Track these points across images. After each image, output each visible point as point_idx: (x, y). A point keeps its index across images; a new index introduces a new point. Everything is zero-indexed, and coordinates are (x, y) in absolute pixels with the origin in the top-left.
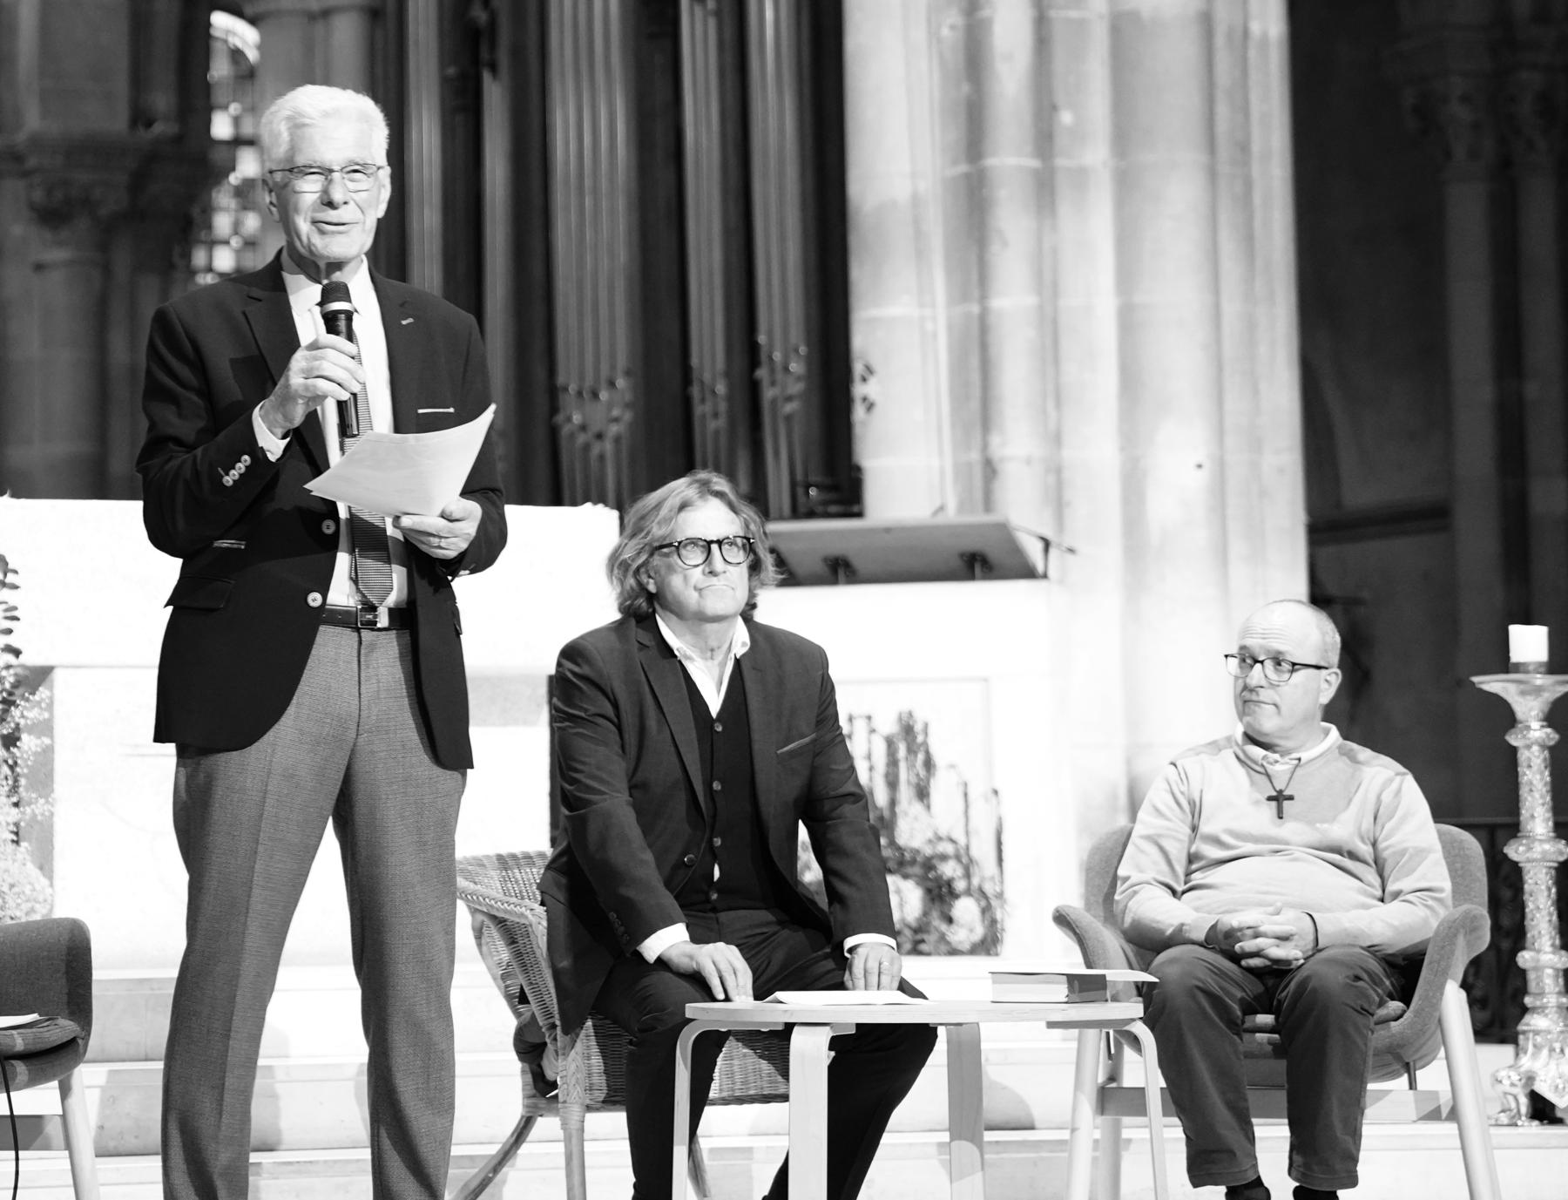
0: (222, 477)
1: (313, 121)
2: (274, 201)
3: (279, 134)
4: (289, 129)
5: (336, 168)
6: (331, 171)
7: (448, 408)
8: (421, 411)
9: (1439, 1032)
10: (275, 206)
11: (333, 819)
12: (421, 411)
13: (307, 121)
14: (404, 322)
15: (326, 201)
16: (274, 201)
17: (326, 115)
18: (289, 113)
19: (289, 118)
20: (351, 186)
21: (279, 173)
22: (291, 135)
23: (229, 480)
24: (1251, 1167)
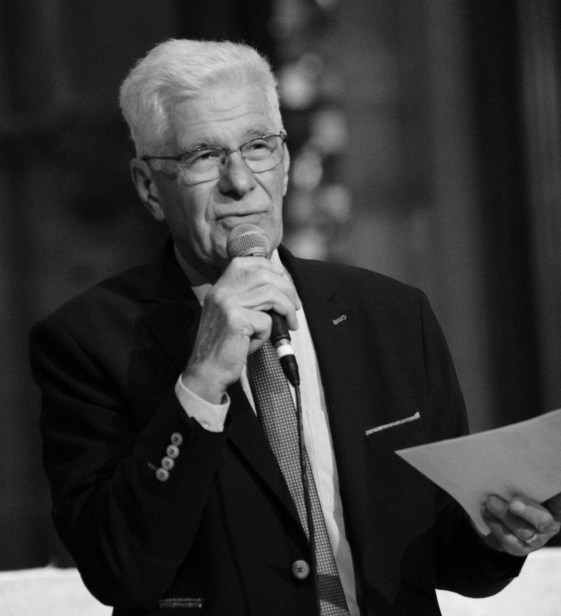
0: (154, 472)
1: (196, 93)
2: (154, 193)
3: (152, 109)
4: (164, 103)
5: (234, 145)
6: (227, 151)
7: (413, 415)
8: (369, 432)
9: (270, 254)
10: (155, 200)
11: (307, 539)
12: (369, 432)
13: (188, 92)
14: (336, 322)
15: (226, 187)
16: (154, 193)
17: (210, 82)
18: (160, 83)
19: (162, 90)
20: (253, 165)
21: (158, 160)
22: (167, 109)
23: (163, 473)
24: (149, 165)
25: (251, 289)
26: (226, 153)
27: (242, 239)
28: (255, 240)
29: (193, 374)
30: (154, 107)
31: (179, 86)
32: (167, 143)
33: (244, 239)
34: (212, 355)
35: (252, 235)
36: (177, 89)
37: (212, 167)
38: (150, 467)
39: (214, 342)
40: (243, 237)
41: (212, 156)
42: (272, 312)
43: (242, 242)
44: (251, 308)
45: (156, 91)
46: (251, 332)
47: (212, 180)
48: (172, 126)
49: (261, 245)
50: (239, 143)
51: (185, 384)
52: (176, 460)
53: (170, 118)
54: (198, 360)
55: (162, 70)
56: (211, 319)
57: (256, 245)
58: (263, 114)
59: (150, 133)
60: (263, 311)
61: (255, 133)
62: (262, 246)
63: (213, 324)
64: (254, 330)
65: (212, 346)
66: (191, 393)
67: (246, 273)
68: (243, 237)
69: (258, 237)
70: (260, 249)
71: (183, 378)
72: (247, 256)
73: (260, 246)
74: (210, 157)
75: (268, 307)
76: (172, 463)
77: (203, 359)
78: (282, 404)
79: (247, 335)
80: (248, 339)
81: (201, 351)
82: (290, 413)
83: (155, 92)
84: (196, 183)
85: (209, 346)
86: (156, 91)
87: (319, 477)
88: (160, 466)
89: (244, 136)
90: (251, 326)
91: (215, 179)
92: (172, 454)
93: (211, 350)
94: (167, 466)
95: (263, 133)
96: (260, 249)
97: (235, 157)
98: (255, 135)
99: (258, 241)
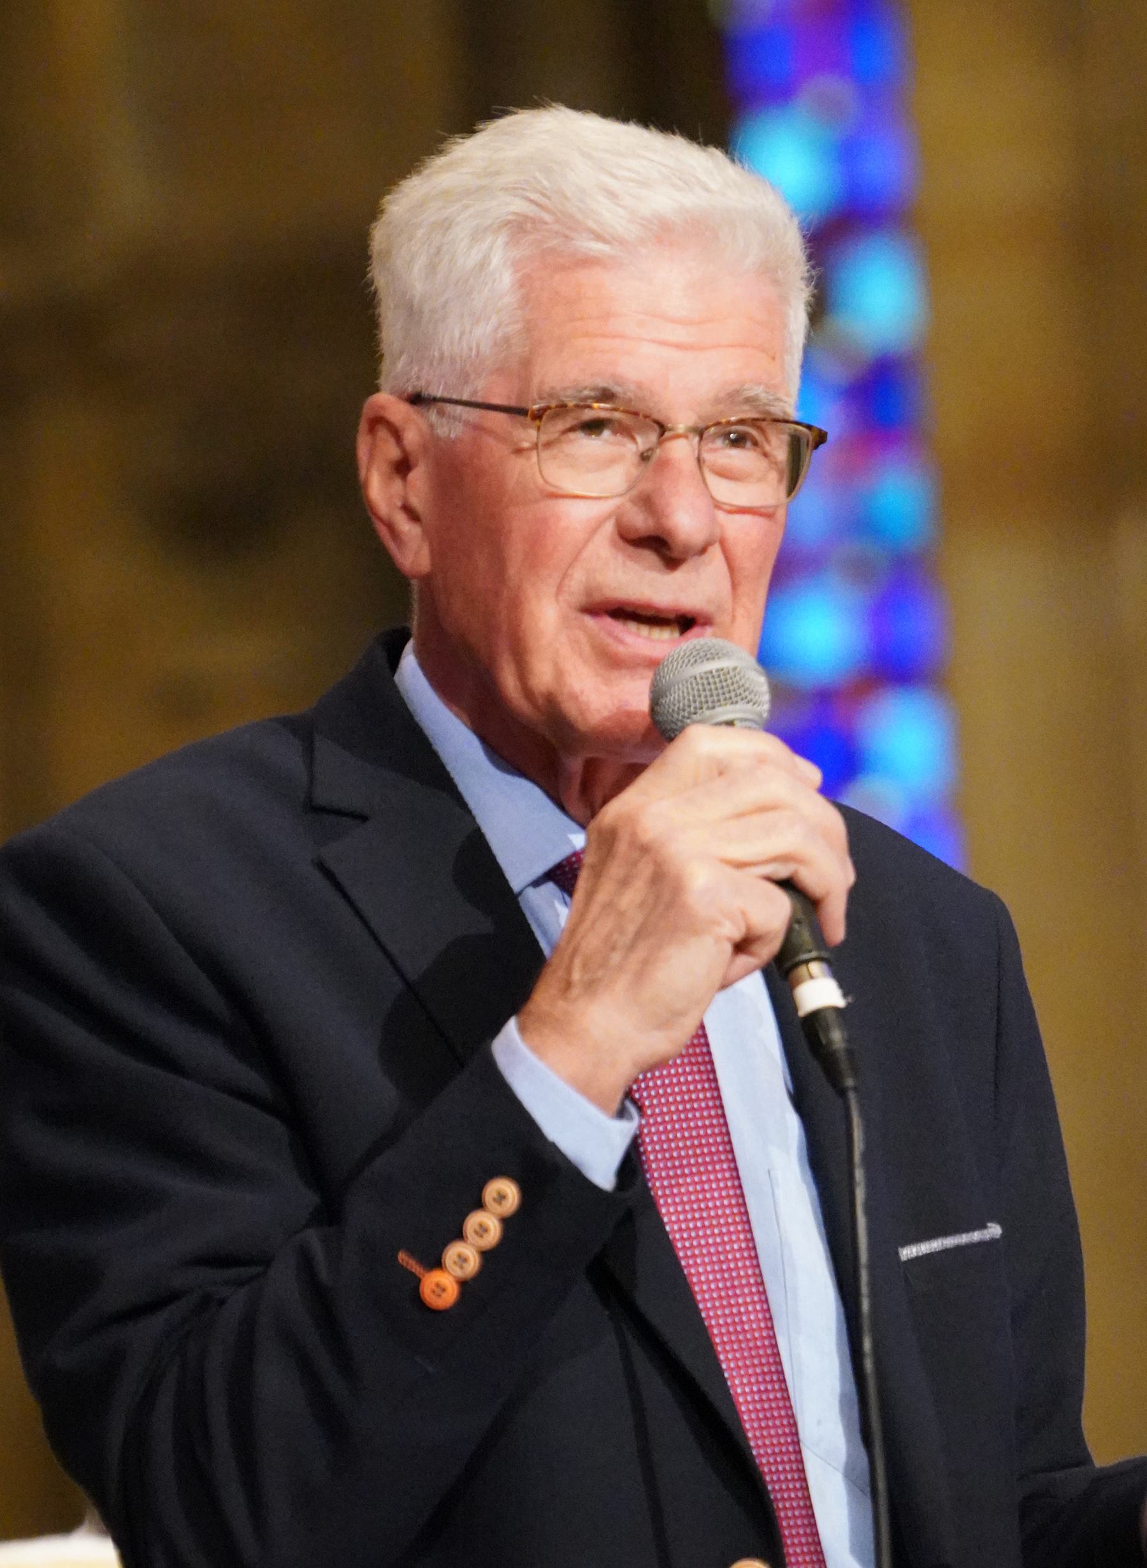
4: (516, 265)
5: (682, 421)
15: (640, 522)
18: (519, 206)
19: (519, 227)
22: (524, 283)
25: (740, 815)
26: (662, 434)
27: (707, 678)
28: (743, 686)
29: (561, 1026)
30: (489, 264)
31: (570, 225)
32: (500, 371)
33: (713, 677)
34: (622, 983)
35: (735, 669)
36: (567, 232)
37: (612, 461)
38: (405, 1264)
39: (632, 947)
40: (711, 672)
41: (615, 432)
42: (788, 885)
43: (707, 687)
44: (740, 865)
45: (506, 225)
46: (737, 934)
47: (607, 498)
48: (529, 328)
49: (749, 698)
50: (700, 417)
51: (535, 1049)
52: (486, 1255)
53: (526, 301)
54: (575, 992)
55: (538, 174)
56: (625, 883)
57: (742, 699)
58: (774, 358)
59: (457, 334)
60: (769, 879)
61: (748, 400)
62: (751, 700)
63: (630, 898)
64: (748, 928)
65: (626, 957)
66: (553, 1078)
67: (721, 769)
68: (711, 672)
69: (739, 674)
70: (744, 712)
71: (522, 1029)
72: (719, 724)
73: (746, 700)
74: (606, 434)
75: (783, 872)
76: (473, 1264)
77: (591, 987)
78: (659, 1082)
79: (729, 939)
80: (728, 948)
81: (585, 966)
82: (668, 1101)
83: (500, 228)
84: (561, 492)
85: (616, 957)
86: (506, 225)
87: (787, 1285)
88: (436, 1263)
89: (717, 401)
90: (743, 913)
91: (612, 497)
92: (481, 1236)
93: (620, 968)
94: (461, 1267)
95: (767, 408)
96: (744, 712)
97: (681, 450)
98: (746, 407)
99: (737, 682)
